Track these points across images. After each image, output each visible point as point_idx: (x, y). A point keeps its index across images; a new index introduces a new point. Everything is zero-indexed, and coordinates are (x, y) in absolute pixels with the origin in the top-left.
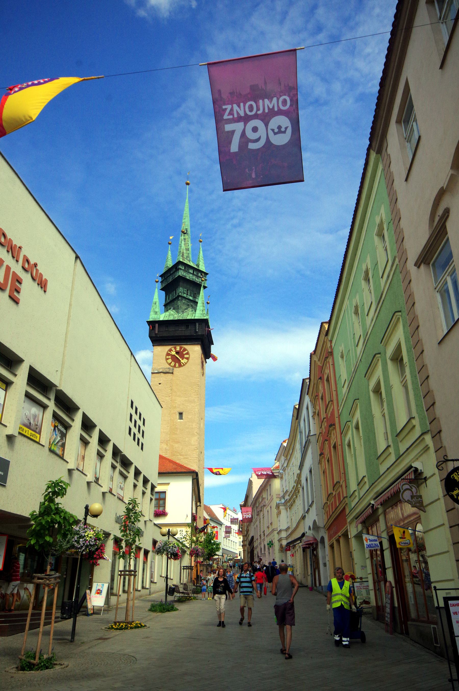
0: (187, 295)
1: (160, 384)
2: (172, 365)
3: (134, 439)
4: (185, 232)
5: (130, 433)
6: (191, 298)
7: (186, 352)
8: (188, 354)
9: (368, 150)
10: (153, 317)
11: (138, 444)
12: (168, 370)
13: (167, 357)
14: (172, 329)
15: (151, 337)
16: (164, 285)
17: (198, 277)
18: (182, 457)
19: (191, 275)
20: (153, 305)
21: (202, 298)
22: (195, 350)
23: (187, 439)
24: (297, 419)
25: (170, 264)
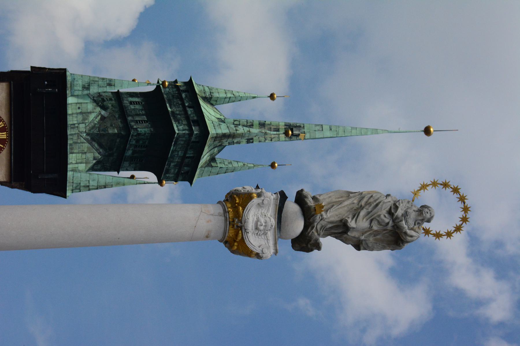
6: (129, 153)
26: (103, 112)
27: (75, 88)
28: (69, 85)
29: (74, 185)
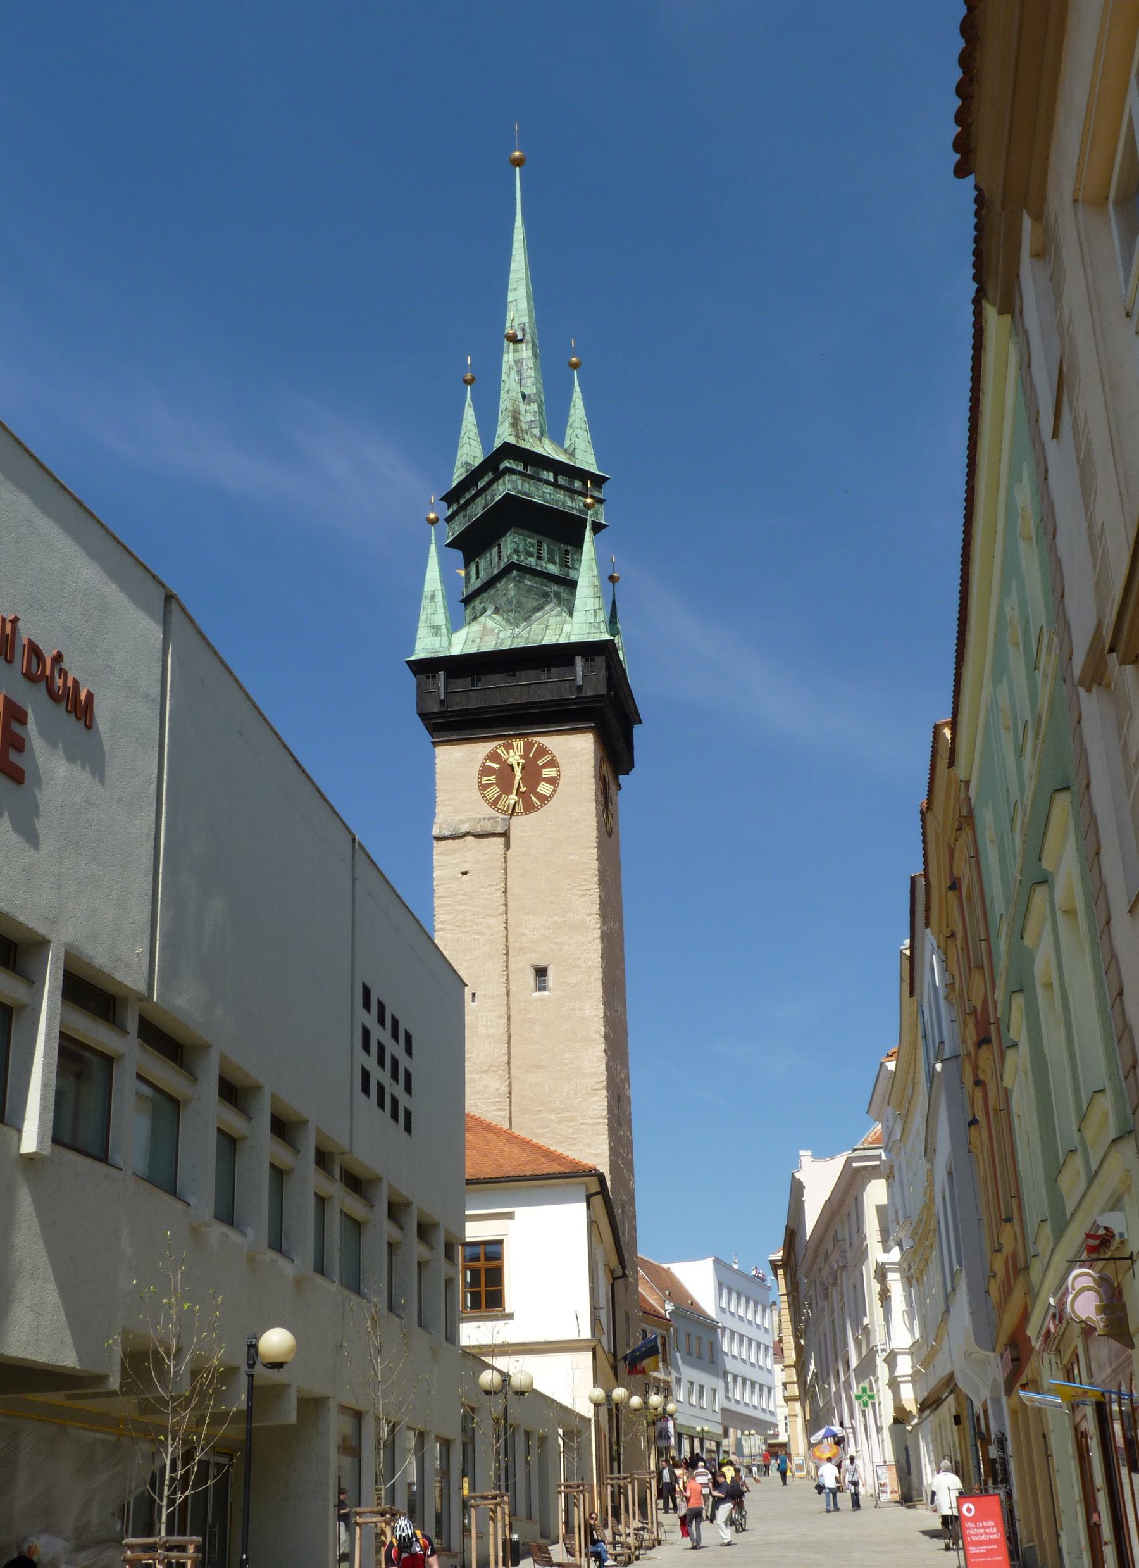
0: (539, 558)
1: (464, 873)
2: (500, 806)
3: (381, 1104)
4: (520, 336)
5: (366, 1089)
6: (553, 569)
7: (548, 757)
8: (553, 763)
9: (977, 302)
10: (426, 646)
11: (395, 1116)
12: (489, 827)
13: (485, 780)
14: (492, 682)
15: (424, 716)
16: (458, 530)
17: (571, 492)
18: (553, 1116)
19: (549, 489)
20: (425, 602)
21: (591, 568)
22: (575, 752)
23: (567, 1055)
24: (912, 994)
25: (470, 451)
26: (488, 612)
27: (437, 646)
28: (432, 655)
29: (593, 631)
